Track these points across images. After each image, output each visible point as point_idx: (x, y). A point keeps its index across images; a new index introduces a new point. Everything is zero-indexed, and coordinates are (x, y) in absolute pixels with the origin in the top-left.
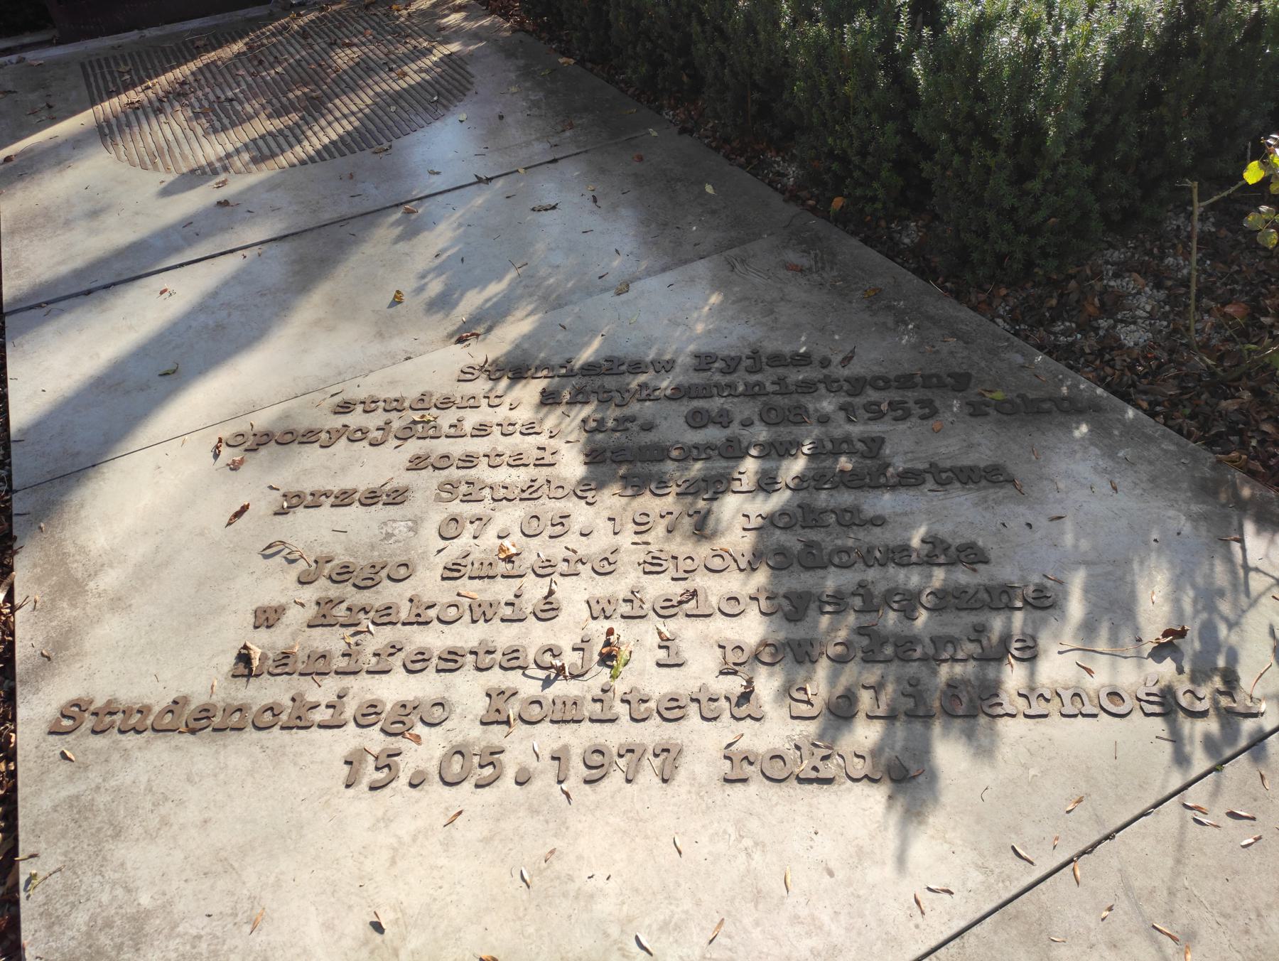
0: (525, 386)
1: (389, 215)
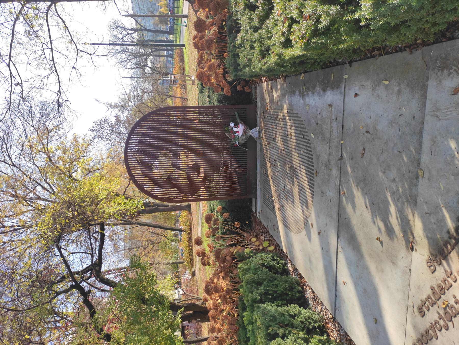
0: (452, 261)
1: (342, 200)
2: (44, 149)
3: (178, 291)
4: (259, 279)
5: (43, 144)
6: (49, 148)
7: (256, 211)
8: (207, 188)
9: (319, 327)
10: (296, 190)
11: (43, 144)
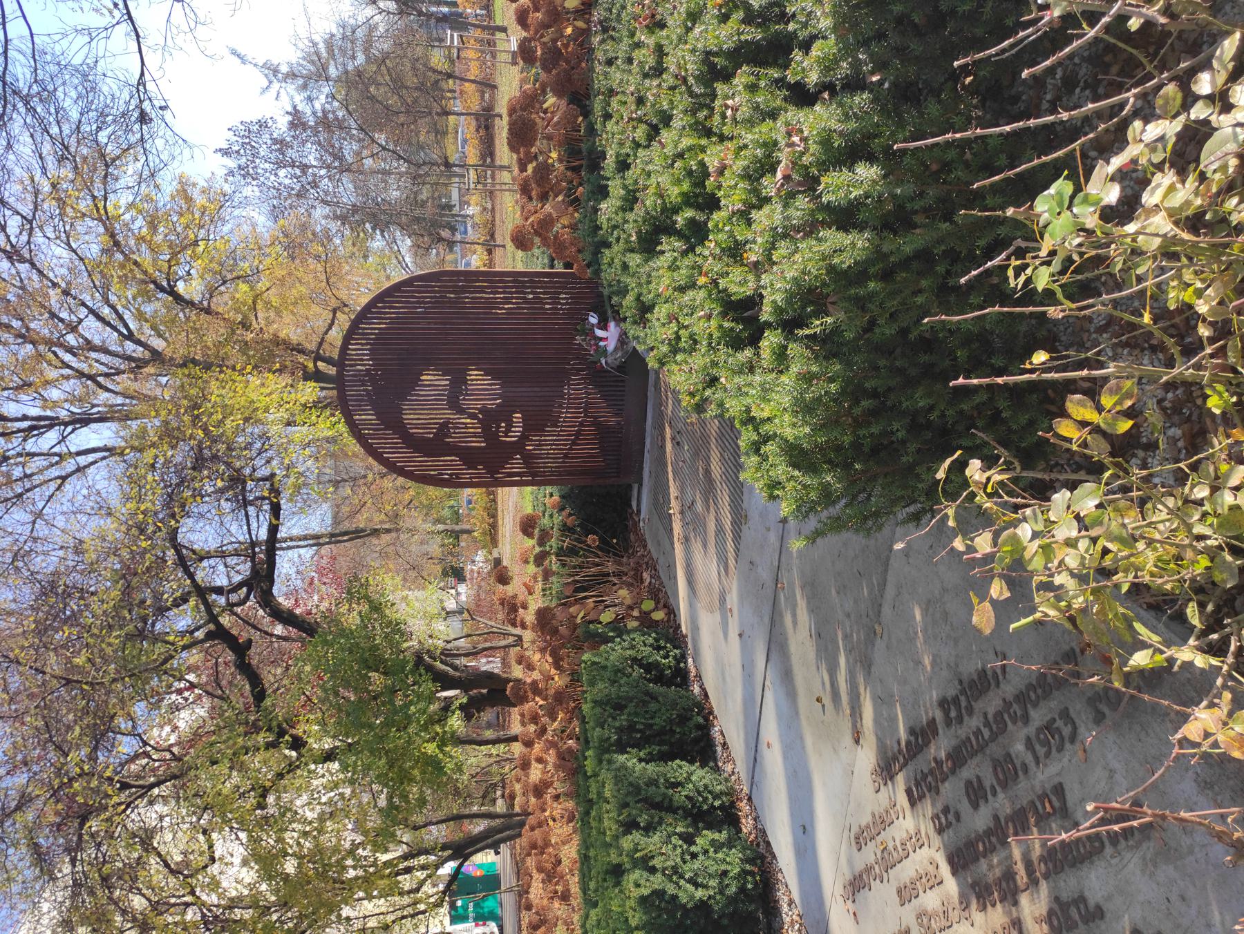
2: (98, 209)
3: (458, 594)
4: (619, 697)
5: (94, 198)
6: (110, 208)
7: (639, 511)
8: (528, 459)
9: (722, 807)
10: (712, 526)
11: (94, 198)
